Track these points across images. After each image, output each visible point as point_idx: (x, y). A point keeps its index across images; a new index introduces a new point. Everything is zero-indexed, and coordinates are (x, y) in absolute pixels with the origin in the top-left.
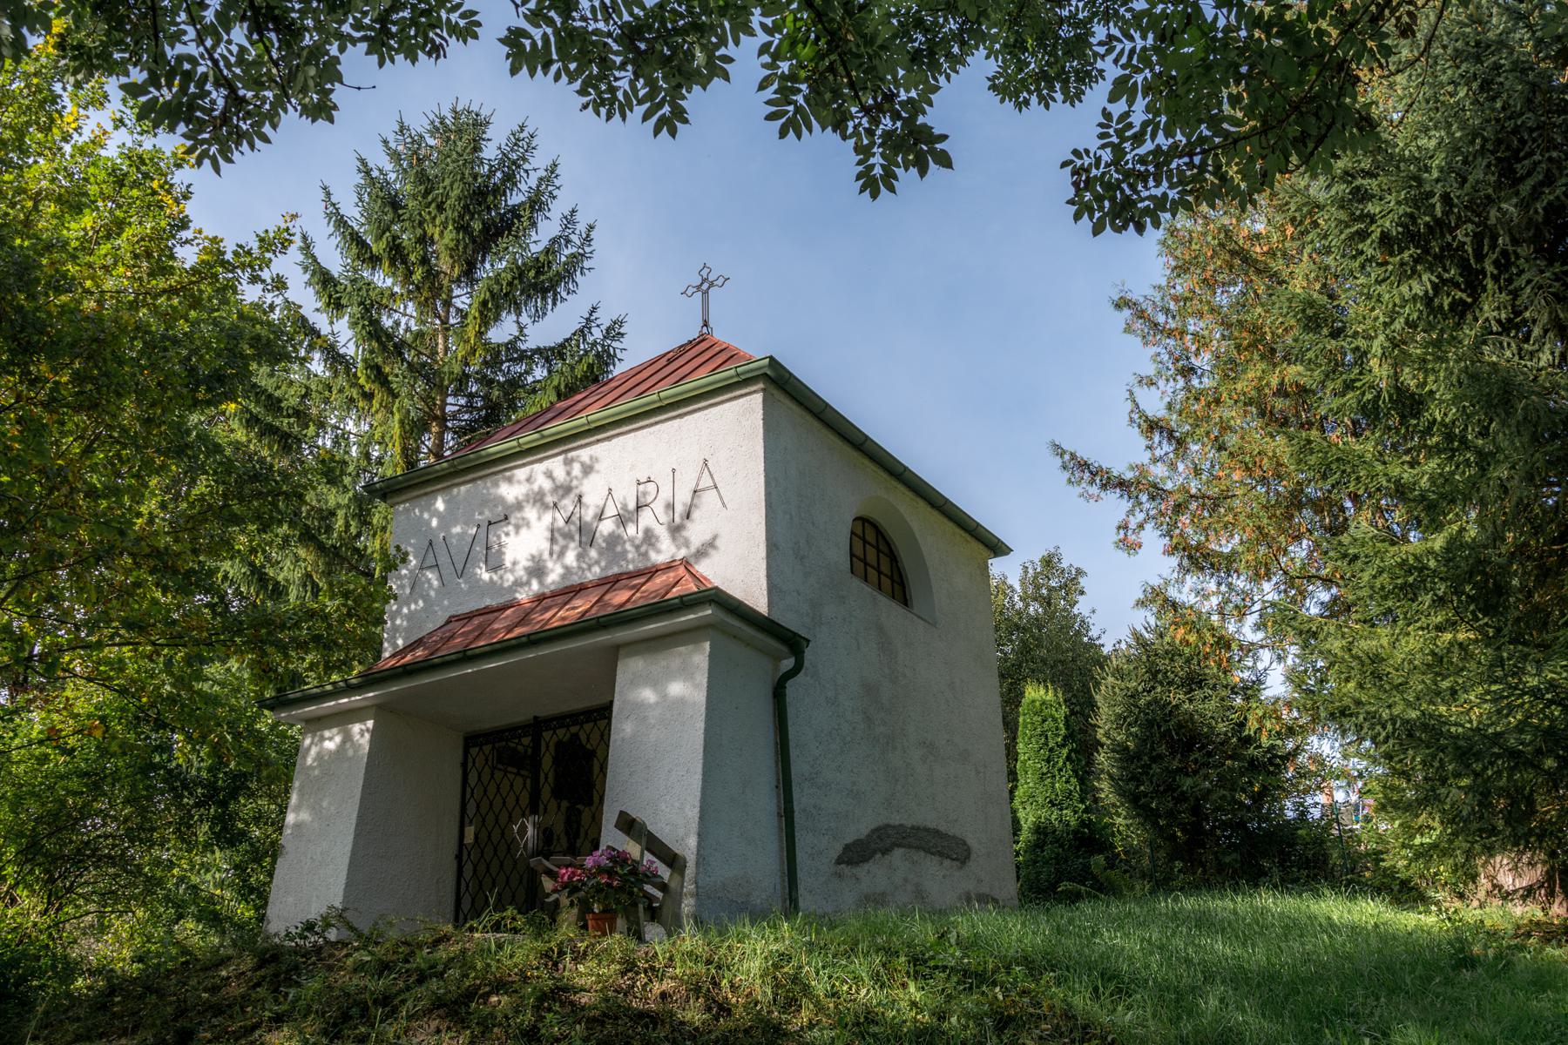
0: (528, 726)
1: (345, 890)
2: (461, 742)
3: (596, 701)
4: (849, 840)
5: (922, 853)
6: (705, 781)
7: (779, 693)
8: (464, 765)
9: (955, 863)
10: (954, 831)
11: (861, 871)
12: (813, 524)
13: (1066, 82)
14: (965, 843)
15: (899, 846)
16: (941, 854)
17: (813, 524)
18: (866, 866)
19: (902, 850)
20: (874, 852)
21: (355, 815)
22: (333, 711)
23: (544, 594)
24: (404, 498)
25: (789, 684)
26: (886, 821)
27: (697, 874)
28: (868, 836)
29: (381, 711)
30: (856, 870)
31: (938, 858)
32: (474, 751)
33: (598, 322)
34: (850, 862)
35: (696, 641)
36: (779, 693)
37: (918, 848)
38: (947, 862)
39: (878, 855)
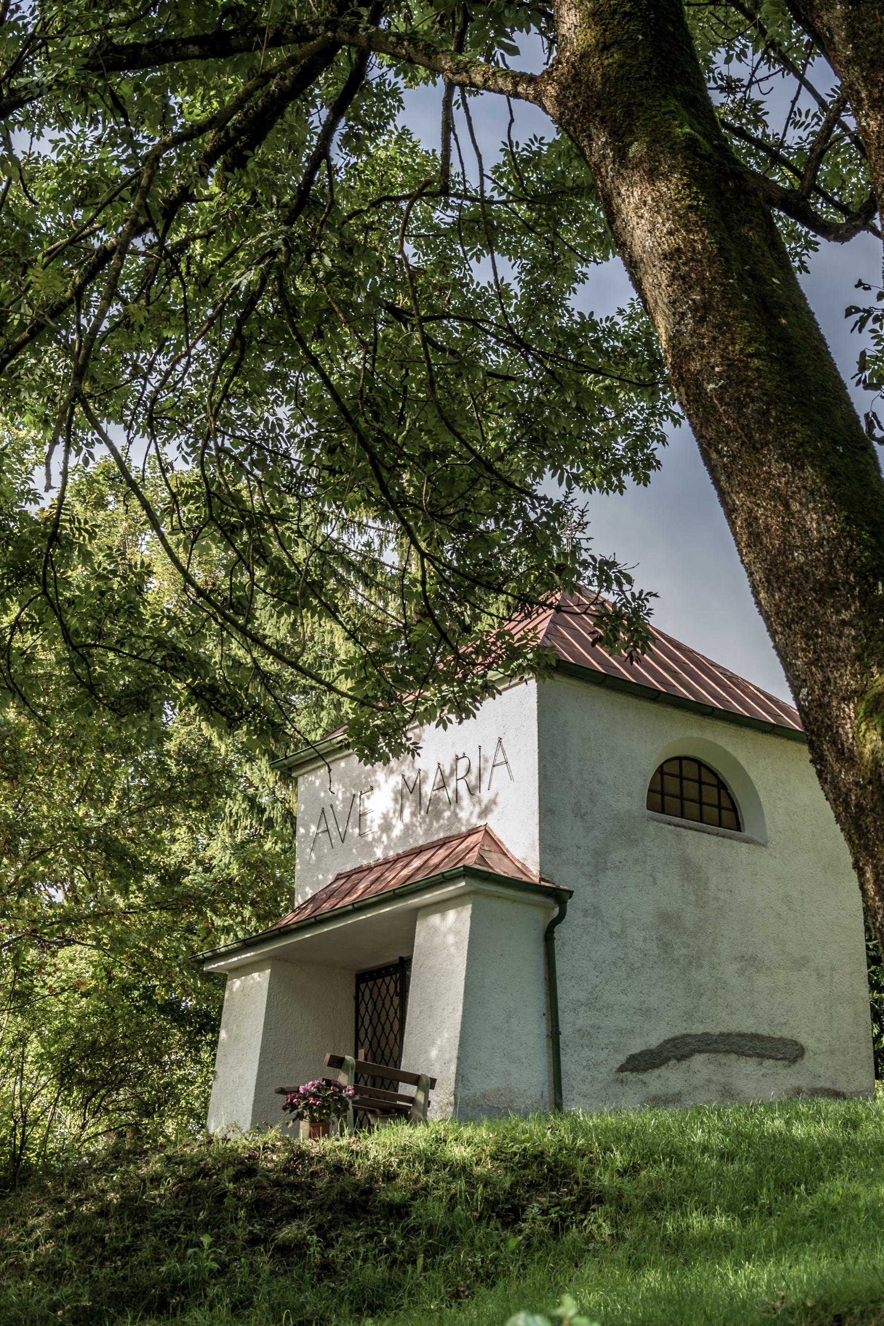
0: (393, 966)
1: (254, 1105)
2: (354, 980)
3: (392, 957)
4: (635, 1050)
5: (733, 1057)
6: (464, 1016)
7: (548, 937)
8: (356, 998)
9: (780, 1063)
10: (786, 1033)
11: (647, 1077)
12: (599, 782)
13: (635, 469)
14: (796, 1043)
15: (701, 1051)
16: (761, 1056)
17: (599, 782)
18: (656, 1072)
19: (704, 1056)
20: (668, 1059)
21: (259, 1047)
22: (240, 964)
23: (398, 855)
24: (303, 771)
25: (556, 928)
26: (684, 1032)
27: (456, 1088)
28: (661, 1046)
29: (276, 961)
30: (644, 1077)
31: (755, 1060)
32: (363, 986)
33: (574, 504)
34: (635, 1069)
35: (463, 904)
36: (548, 937)
37: (727, 1052)
38: (768, 1063)
39: (673, 1062)
